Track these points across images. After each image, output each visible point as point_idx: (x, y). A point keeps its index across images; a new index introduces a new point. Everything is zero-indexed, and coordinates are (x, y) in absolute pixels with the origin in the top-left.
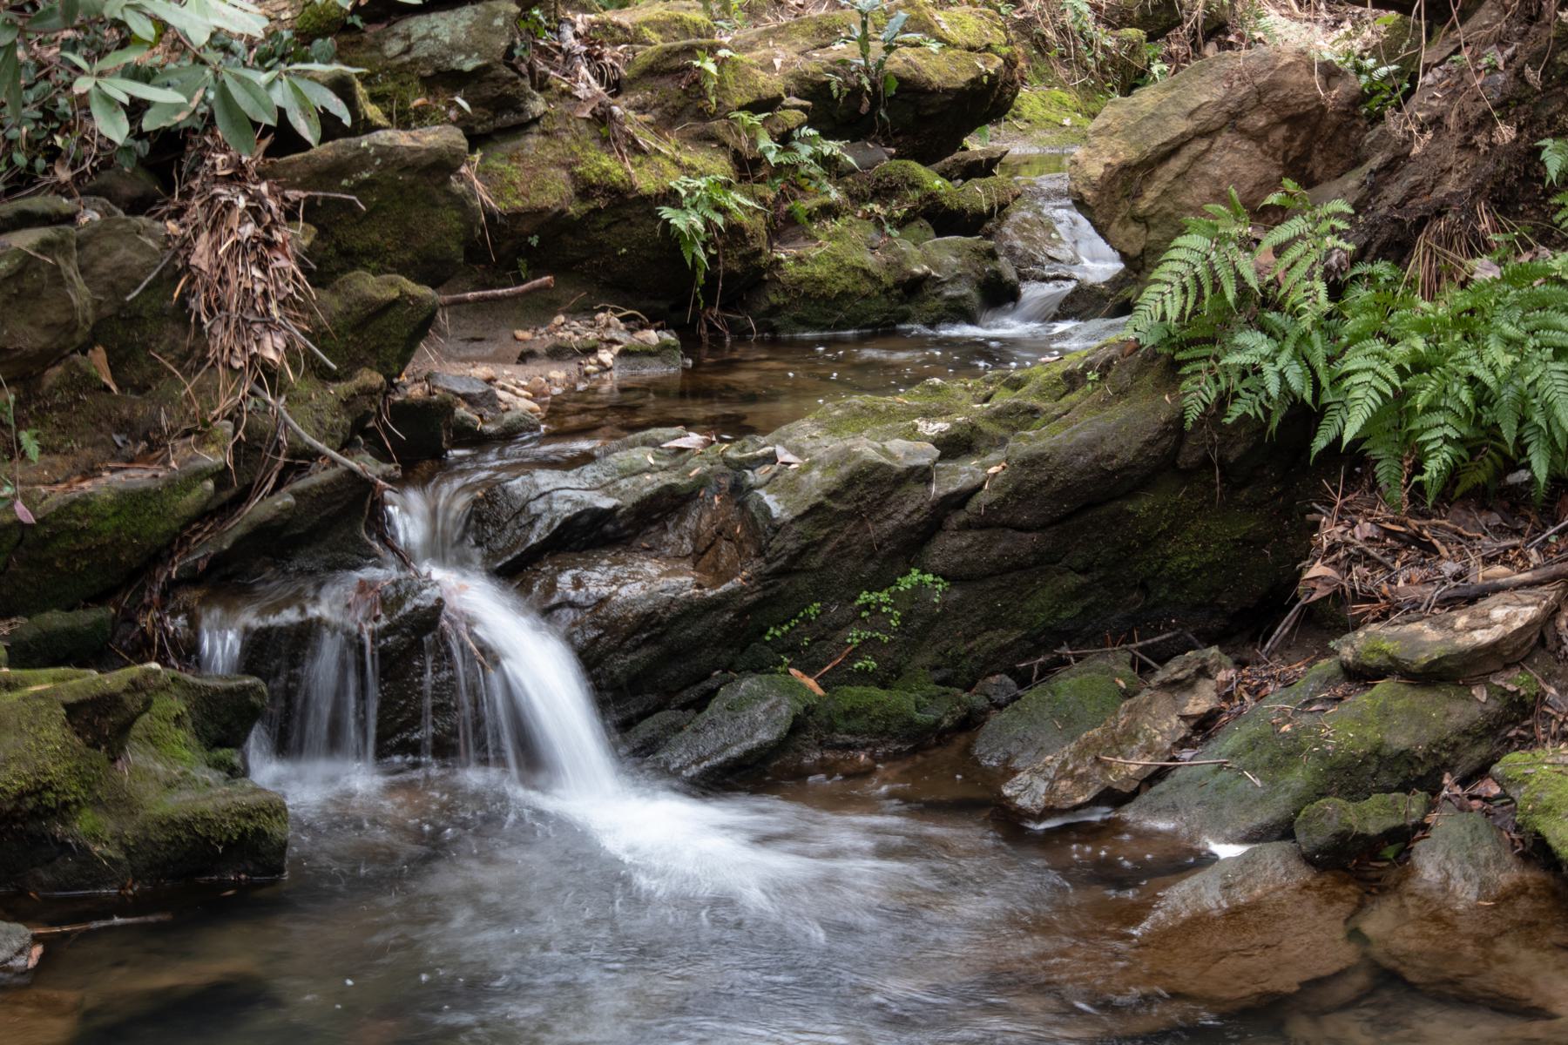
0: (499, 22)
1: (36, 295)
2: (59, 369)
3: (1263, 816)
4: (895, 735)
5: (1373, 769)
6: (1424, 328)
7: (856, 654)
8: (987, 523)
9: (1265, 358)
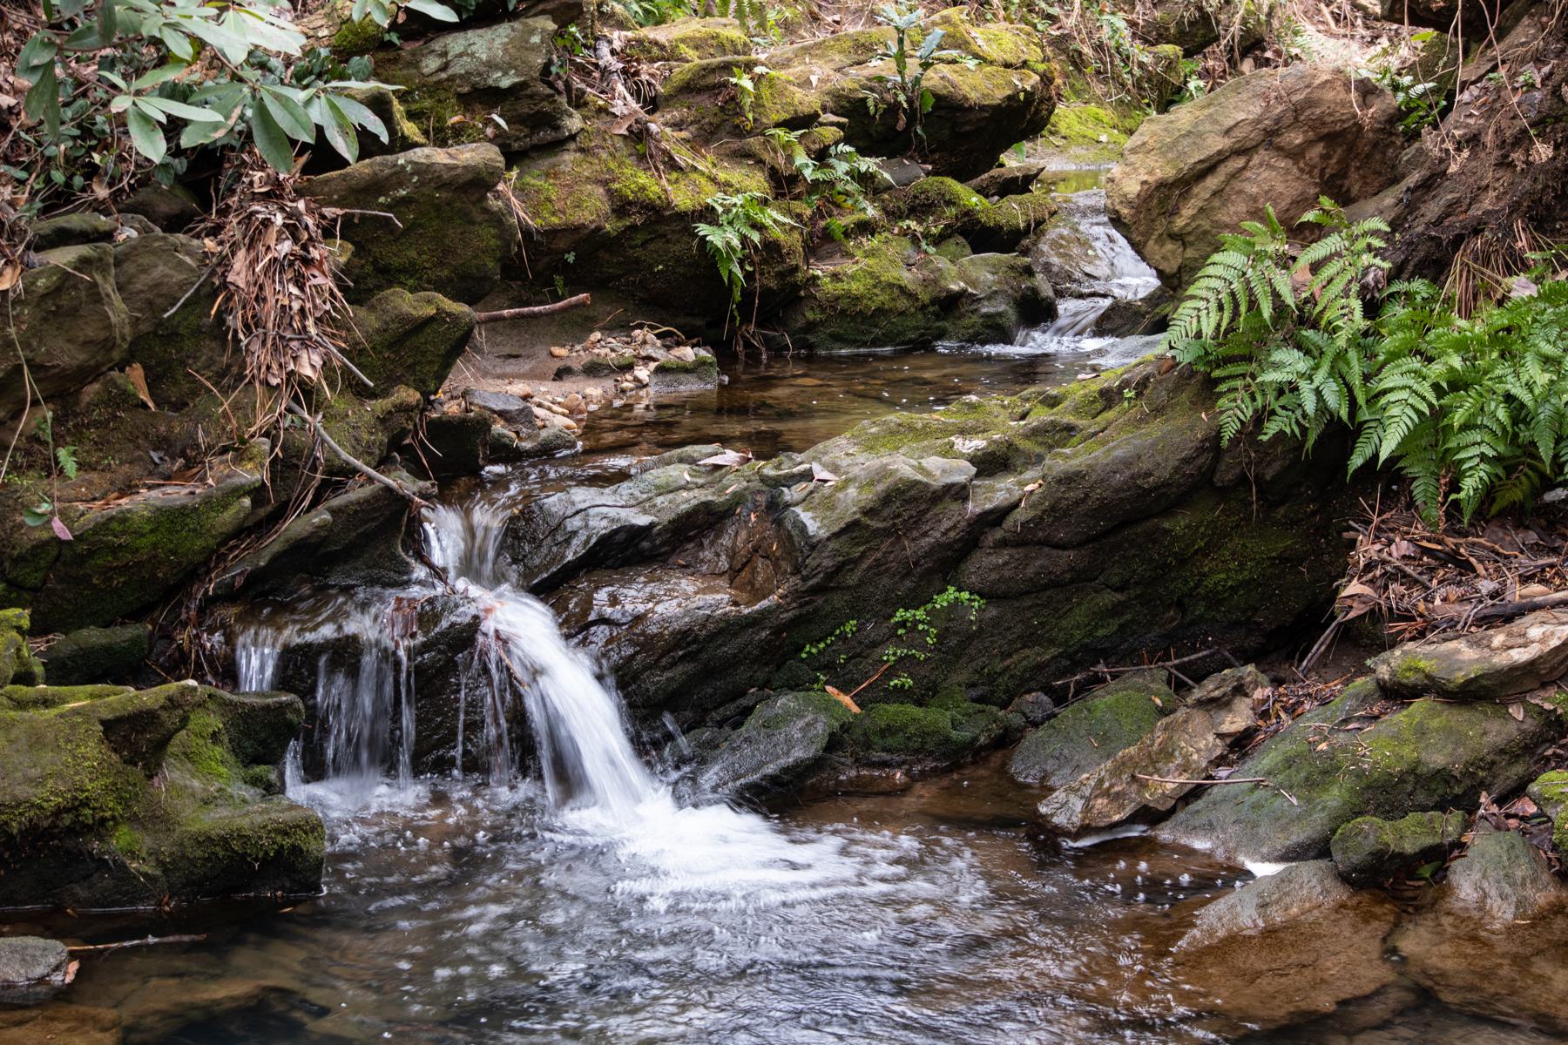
0: (536, 39)
1: (74, 312)
2: (96, 386)
4: (931, 753)
5: (1409, 788)
6: (1461, 346)
7: (892, 672)
8: (1023, 540)
9: (1301, 375)
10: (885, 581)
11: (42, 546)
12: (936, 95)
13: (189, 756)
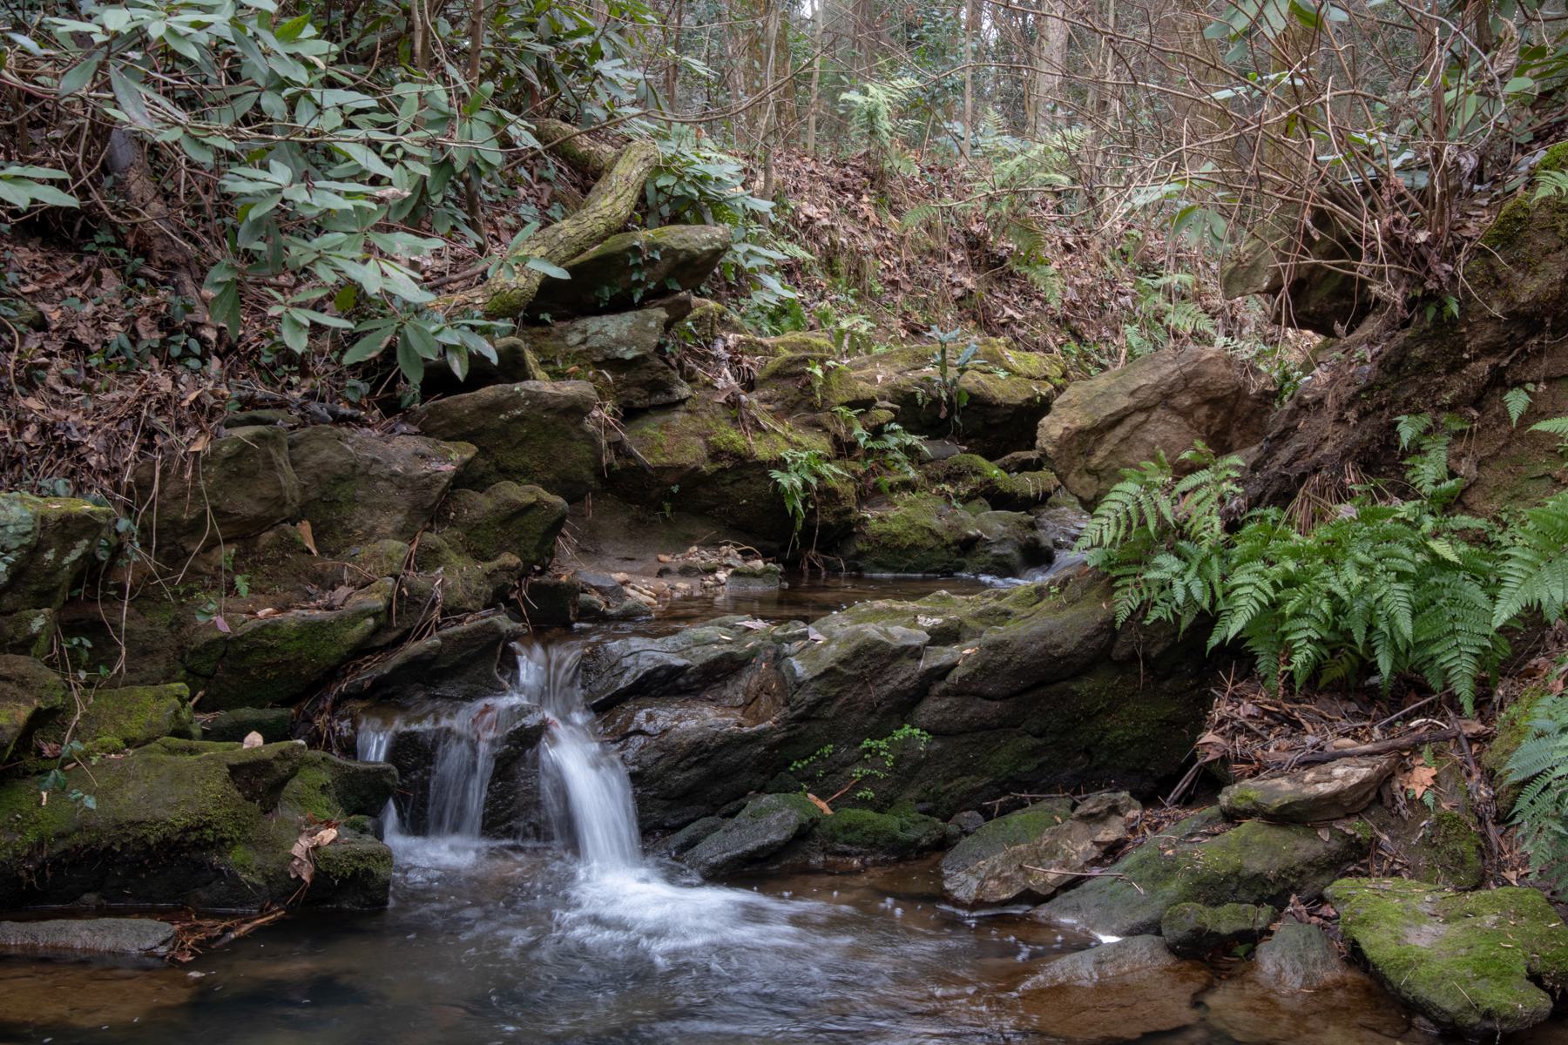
0: (652, 324)
1: (253, 475)
2: (271, 533)
3: (1143, 916)
4: (882, 848)
5: (1233, 887)
6: (1295, 554)
7: (859, 786)
8: (960, 691)
9: (1175, 575)
10: (855, 716)
11: (212, 643)
12: (969, 393)
13: (301, 801)
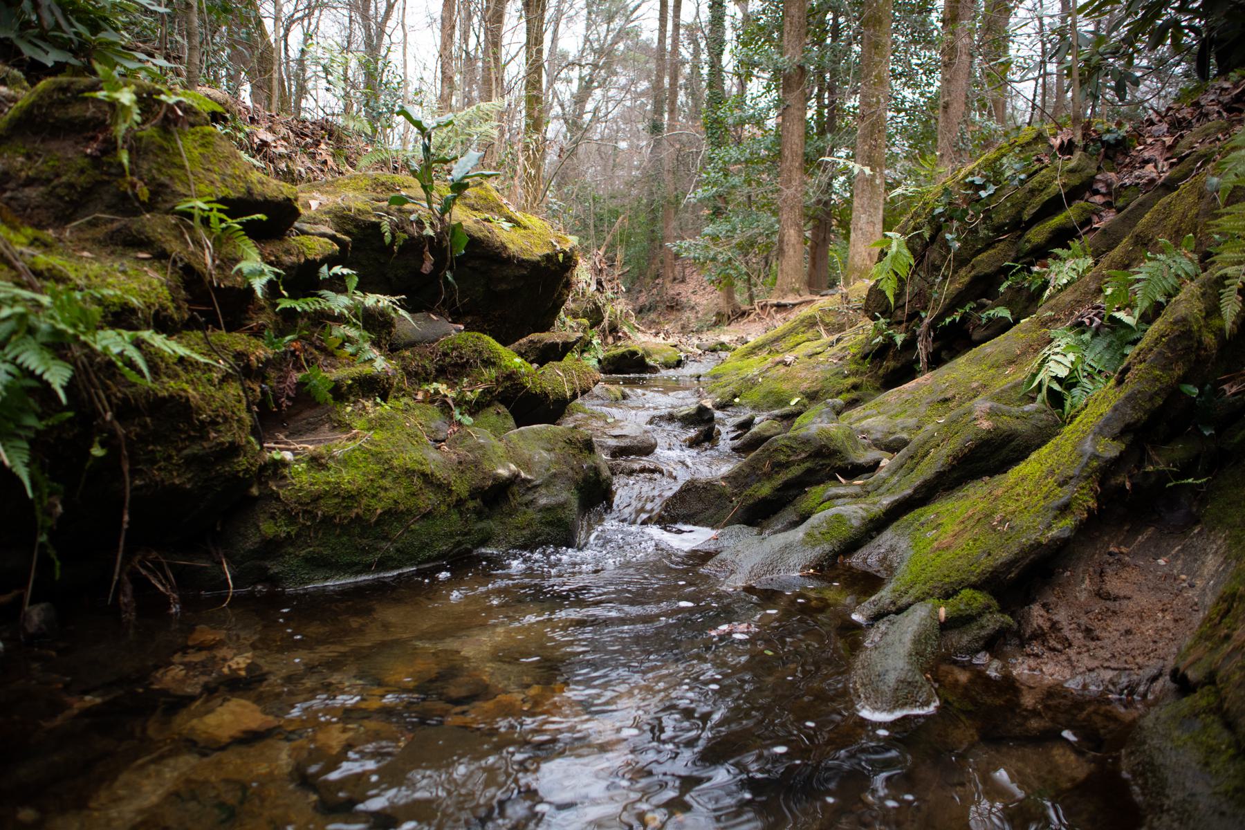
12: (470, 236)
